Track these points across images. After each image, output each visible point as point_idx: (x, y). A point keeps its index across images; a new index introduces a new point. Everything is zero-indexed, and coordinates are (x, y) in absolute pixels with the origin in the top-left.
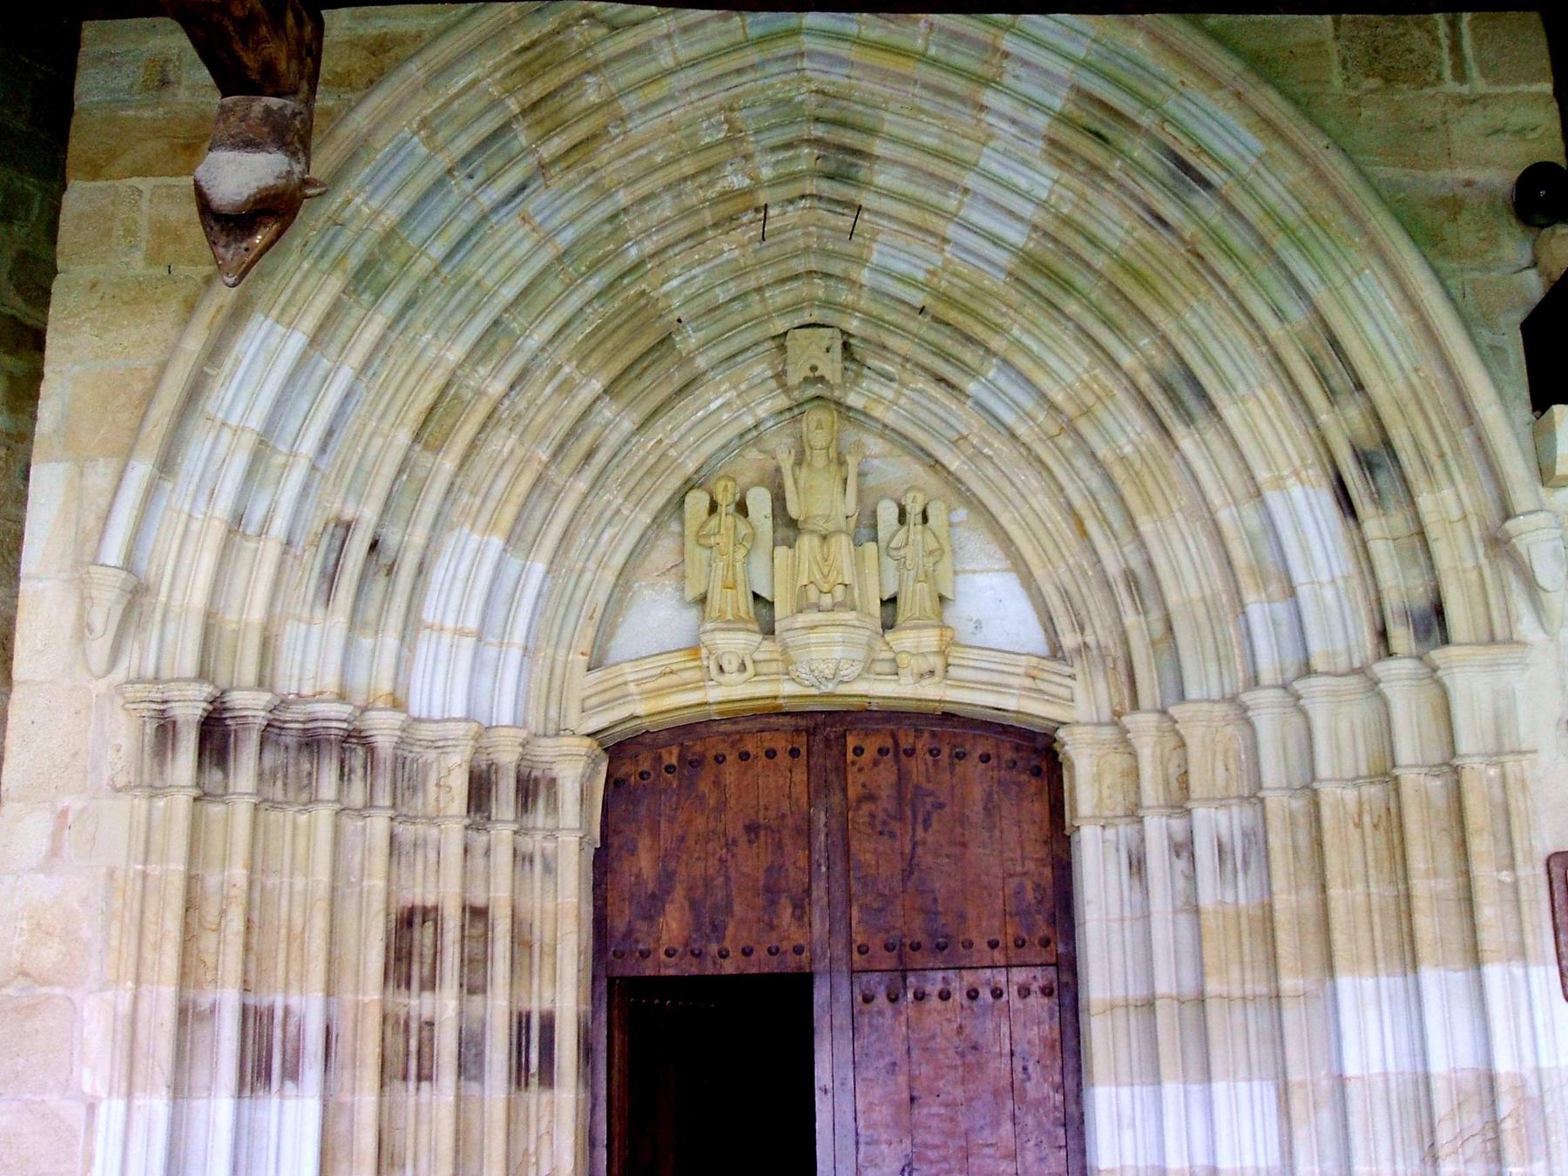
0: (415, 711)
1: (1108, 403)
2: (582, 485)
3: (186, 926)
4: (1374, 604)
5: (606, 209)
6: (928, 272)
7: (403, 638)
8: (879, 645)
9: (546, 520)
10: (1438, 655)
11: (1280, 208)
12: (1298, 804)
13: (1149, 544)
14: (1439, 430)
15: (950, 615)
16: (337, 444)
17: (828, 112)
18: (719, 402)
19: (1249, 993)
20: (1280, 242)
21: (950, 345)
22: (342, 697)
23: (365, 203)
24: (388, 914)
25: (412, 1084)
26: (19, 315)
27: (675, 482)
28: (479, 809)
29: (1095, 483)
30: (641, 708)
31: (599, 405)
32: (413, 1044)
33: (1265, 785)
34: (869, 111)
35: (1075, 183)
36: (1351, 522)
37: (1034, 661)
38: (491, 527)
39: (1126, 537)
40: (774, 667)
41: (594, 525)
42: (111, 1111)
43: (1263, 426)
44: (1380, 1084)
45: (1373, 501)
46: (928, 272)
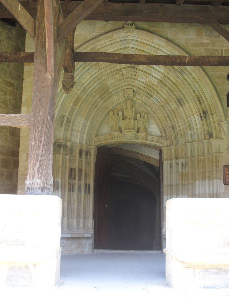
2: (95, 110)
25: (71, 192)
26: (10, 81)
27: (108, 110)
30: (103, 142)
35: (167, 71)
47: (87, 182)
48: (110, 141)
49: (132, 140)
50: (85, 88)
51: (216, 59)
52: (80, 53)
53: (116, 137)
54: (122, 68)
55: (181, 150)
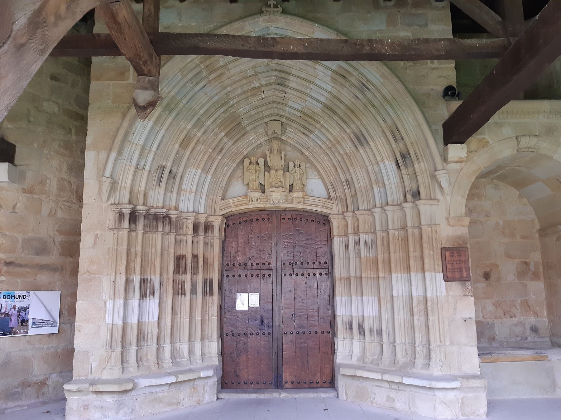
0: (180, 210)
1: (343, 140)
2: (219, 157)
3: (127, 261)
4: (404, 190)
5: (225, 91)
6: (302, 108)
7: (177, 194)
8: (289, 195)
9: (211, 166)
10: (418, 202)
11: (386, 95)
12: (385, 234)
13: (352, 174)
14: (421, 149)
15: (305, 189)
16: (161, 148)
17: (279, 68)
18: (252, 138)
19: (372, 276)
20: (385, 104)
21: (307, 125)
22: (163, 207)
23: (166, 89)
24: (174, 257)
26: (77, 111)
27: (242, 157)
28: (196, 232)
29: (340, 159)
30: (234, 209)
31: (224, 138)
32: (180, 286)
33: (376, 230)
34: (289, 68)
35: (337, 87)
36: (399, 170)
37: (324, 200)
38: (198, 167)
39: (346, 171)
40: (264, 200)
41: (223, 166)
42: (110, 303)
43: (380, 147)
44: (401, 298)
45: (404, 165)
46: (302, 108)
47: (208, 276)
48: (246, 207)
49: (280, 205)
50: (199, 119)
51: (442, 45)
52: (168, 36)
53: (256, 200)
54: (262, 86)
55: (363, 219)
